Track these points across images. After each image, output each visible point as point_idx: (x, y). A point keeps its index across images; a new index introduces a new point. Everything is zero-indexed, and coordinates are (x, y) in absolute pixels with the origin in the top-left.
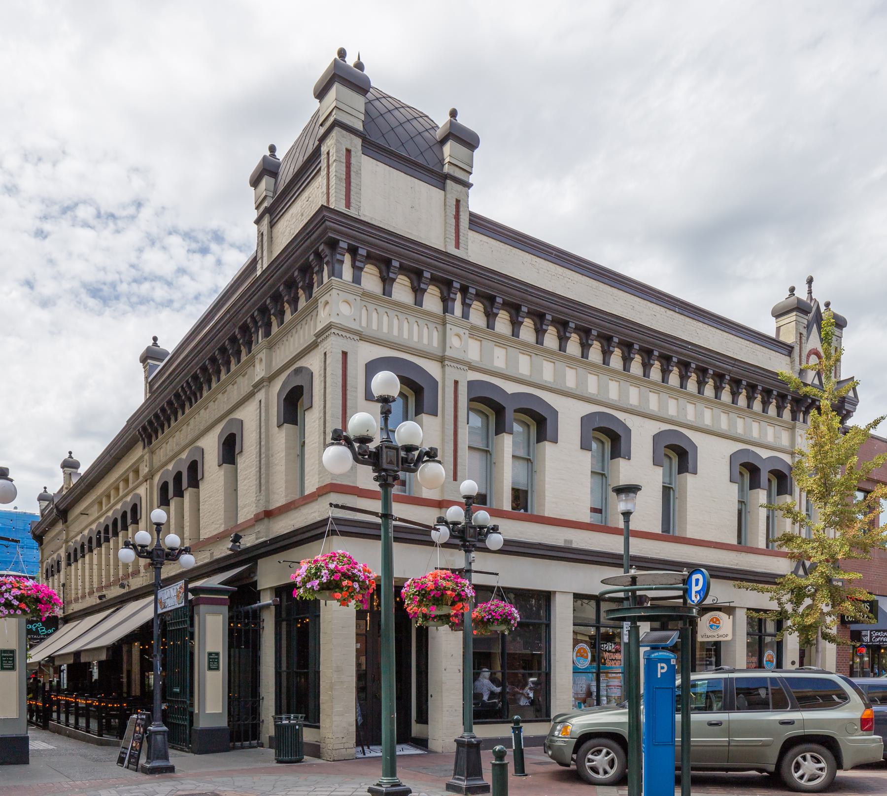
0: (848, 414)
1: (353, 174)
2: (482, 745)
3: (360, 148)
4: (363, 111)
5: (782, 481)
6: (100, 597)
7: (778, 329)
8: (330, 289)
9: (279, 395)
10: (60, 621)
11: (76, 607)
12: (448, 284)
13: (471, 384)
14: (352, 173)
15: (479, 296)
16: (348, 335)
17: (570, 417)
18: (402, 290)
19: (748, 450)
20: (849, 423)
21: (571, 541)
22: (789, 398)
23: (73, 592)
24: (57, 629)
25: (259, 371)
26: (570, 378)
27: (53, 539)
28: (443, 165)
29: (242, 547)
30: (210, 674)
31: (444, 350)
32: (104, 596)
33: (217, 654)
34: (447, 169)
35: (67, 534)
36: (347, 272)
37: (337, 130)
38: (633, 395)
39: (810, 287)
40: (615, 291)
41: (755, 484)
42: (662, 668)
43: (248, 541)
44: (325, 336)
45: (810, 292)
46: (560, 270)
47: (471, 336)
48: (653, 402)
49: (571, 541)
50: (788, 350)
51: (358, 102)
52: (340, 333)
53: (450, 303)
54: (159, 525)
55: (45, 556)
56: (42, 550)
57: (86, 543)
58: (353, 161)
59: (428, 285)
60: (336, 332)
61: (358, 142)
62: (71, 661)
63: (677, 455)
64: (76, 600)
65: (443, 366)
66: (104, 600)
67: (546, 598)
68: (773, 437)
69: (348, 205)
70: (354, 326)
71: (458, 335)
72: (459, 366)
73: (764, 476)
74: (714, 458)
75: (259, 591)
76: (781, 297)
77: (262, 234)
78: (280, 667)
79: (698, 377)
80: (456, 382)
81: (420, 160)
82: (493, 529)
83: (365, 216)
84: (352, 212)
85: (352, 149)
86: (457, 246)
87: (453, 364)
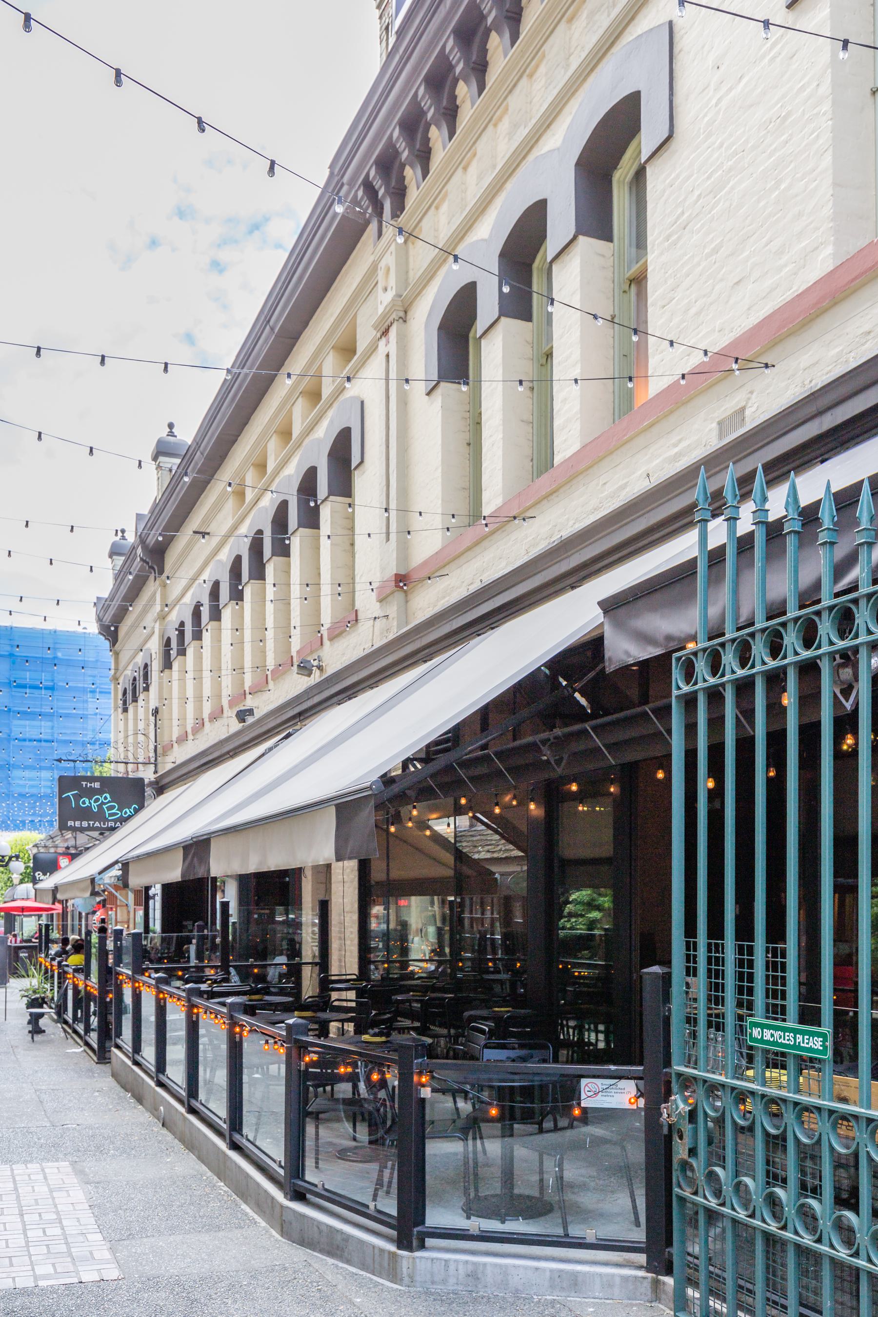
6: (242, 716)
10: (149, 791)
11: (180, 755)
23: (175, 722)
24: (142, 807)
27: (135, 626)
32: (251, 712)
35: (164, 596)
55: (121, 667)
56: (117, 654)
57: (206, 601)
62: (175, 875)
64: (183, 739)
66: (250, 720)
77: (169, 639)
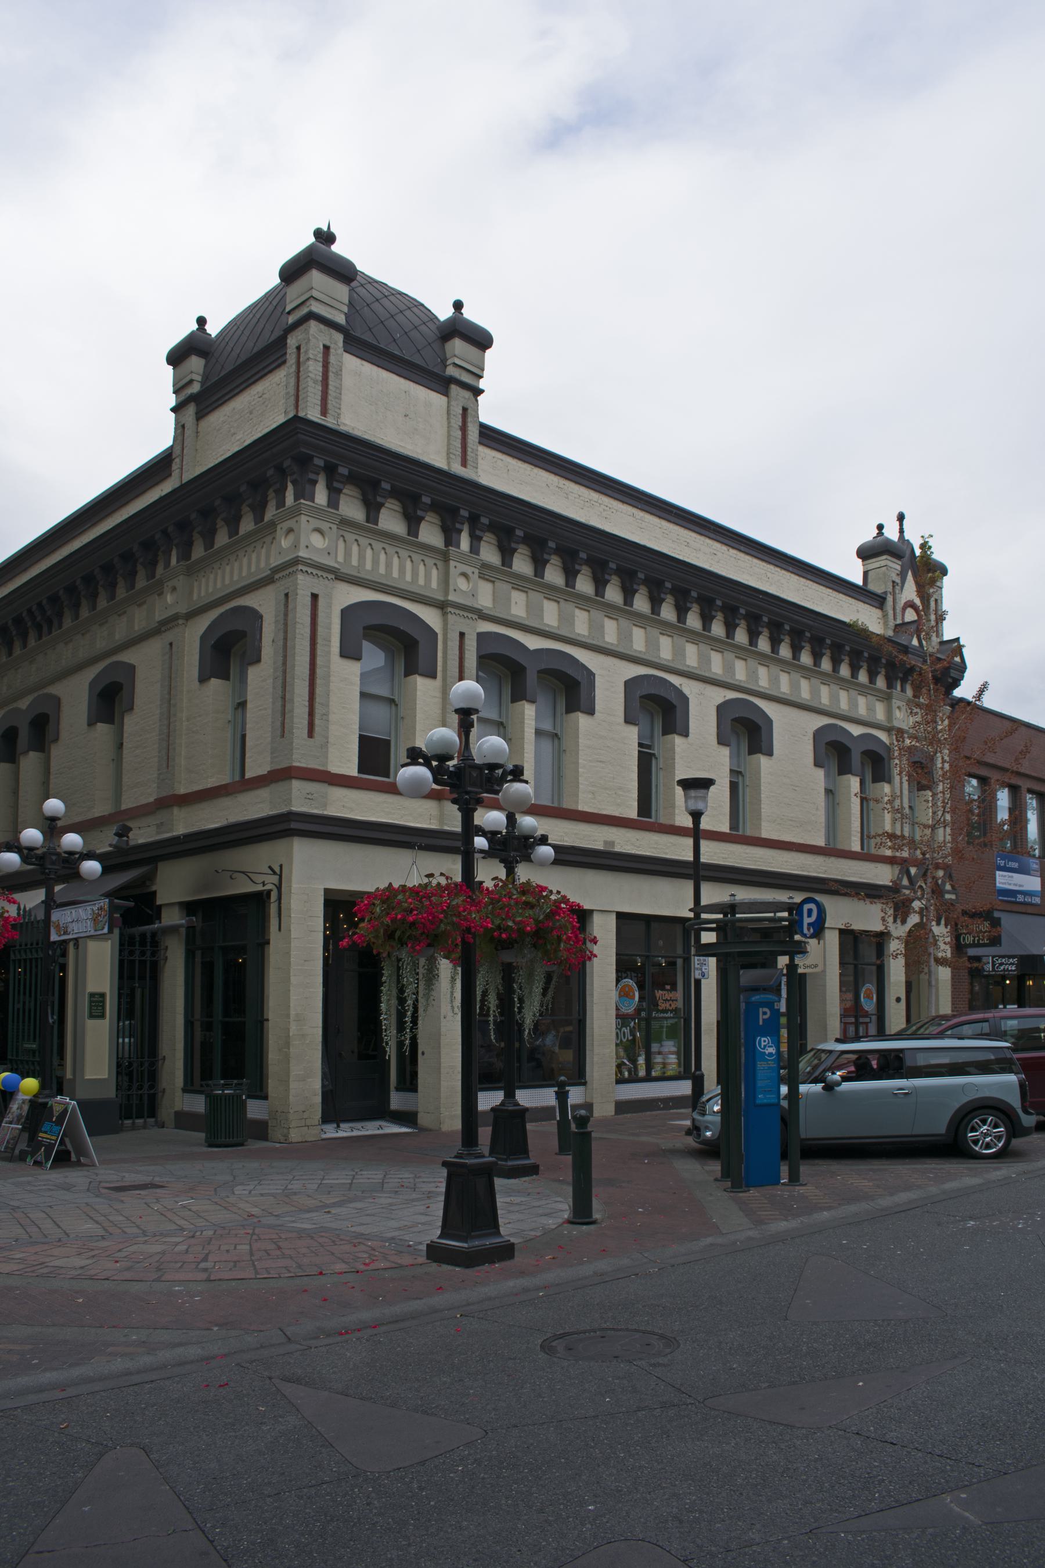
0: (956, 683)
1: (331, 375)
2: (527, 1115)
3: (341, 344)
4: (347, 302)
5: (876, 764)
7: (866, 574)
8: (295, 512)
9: (203, 638)
12: (454, 512)
13: (481, 636)
14: (331, 374)
15: (493, 528)
16: (320, 573)
17: (610, 681)
18: (391, 521)
19: (835, 725)
20: (957, 693)
21: (612, 843)
22: (884, 661)
25: (170, 602)
26: (611, 632)
28: (446, 366)
29: (132, 843)
30: (91, 1024)
31: (446, 592)
33: (103, 995)
34: (451, 371)
36: (321, 496)
37: (313, 323)
38: (691, 655)
39: (901, 525)
40: (664, 523)
41: (844, 769)
42: (765, 1013)
43: (142, 834)
44: (287, 572)
45: (901, 531)
46: (595, 496)
47: (482, 576)
48: (716, 664)
49: (612, 843)
50: (878, 600)
51: (341, 291)
52: (310, 570)
53: (454, 535)
54: (53, 819)
58: (332, 359)
59: (426, 511)
60: (305, 569)
61: (339, 338)
63: (746, 730)
65: (444, 614)
67: (583, 916)
68: (871, 711)
69: (324, 412)
70: (329, 562)
71: (464, 575)
72: (466, 614)
73: (856, 758)
74: (793, 734)
75: (160, 907)
76: (869, 535)
78: (193, 1016)
79: (771, 633)
80: (462, 635)
81: (418, 361)
82: (540, 839)
83: (345, 425)
84: (330, 422)
85: (332, 346)
86: (464, 463)
87: (457, 612)
